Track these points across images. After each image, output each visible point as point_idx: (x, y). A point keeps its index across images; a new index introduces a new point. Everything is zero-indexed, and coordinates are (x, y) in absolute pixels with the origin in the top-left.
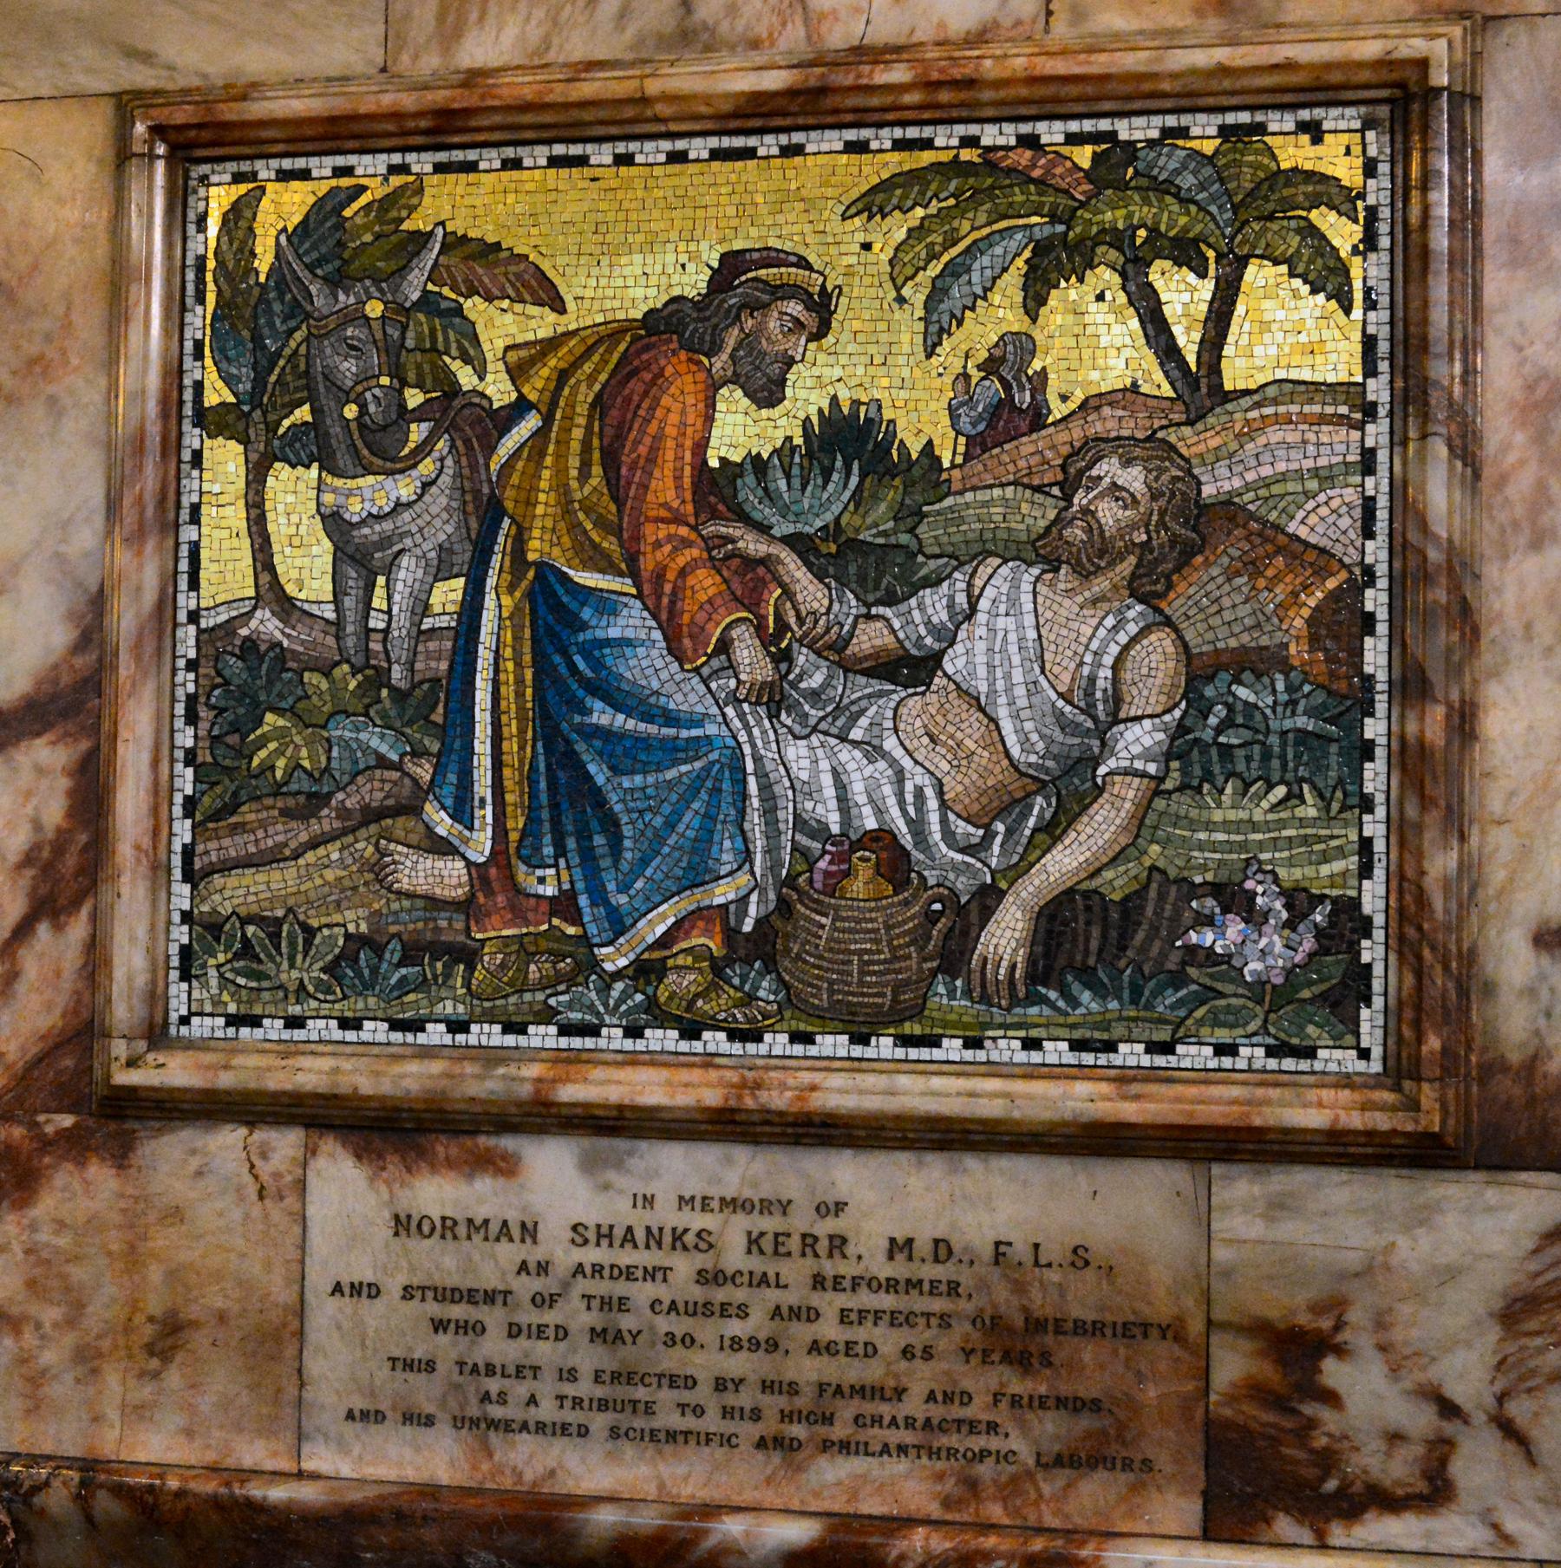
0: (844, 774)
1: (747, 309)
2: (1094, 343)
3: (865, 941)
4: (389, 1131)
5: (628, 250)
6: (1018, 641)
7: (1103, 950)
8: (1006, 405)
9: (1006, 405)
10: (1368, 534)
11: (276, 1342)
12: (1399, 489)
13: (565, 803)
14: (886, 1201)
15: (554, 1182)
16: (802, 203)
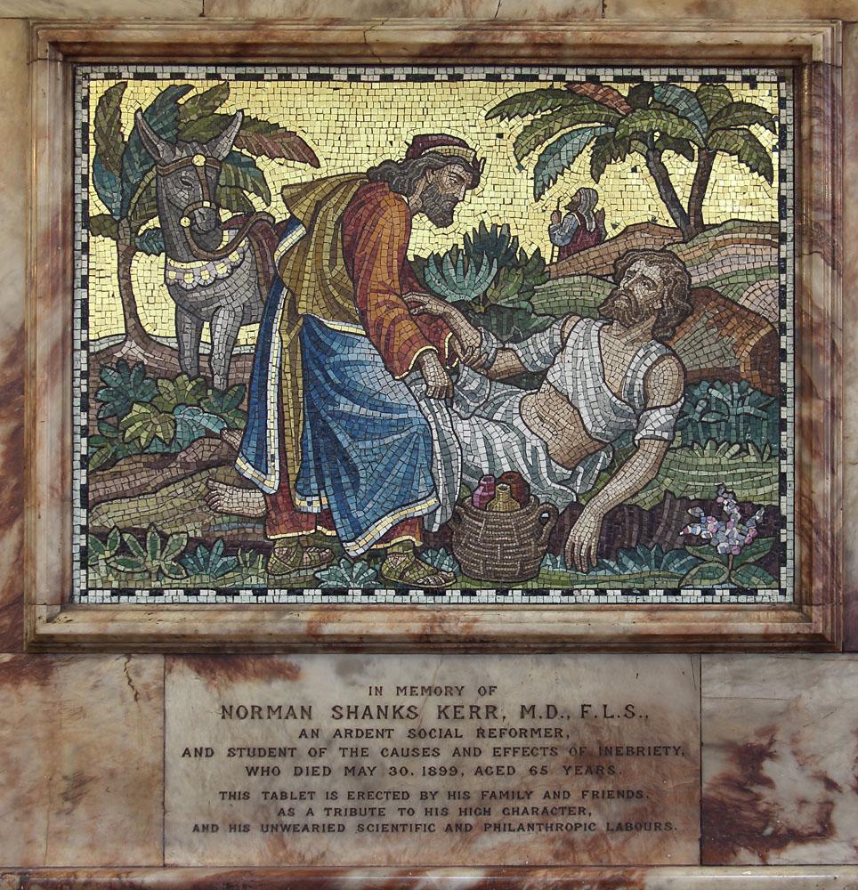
0: (494, 439)
1: (433, 167)
2: (628, 197)
3: (502, 534)
4: (215, 656)
5: (352, 127)
6: (591, 366)
7: (637, 535)
8: (581, 227)
9: (581, 227)
10: (783, 305)
11: (148, 787)
12: (798, 281)
13: (324, 455)
14: (518, 684)
15: (321, 681)
16: (461, 109)
